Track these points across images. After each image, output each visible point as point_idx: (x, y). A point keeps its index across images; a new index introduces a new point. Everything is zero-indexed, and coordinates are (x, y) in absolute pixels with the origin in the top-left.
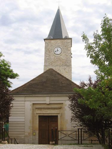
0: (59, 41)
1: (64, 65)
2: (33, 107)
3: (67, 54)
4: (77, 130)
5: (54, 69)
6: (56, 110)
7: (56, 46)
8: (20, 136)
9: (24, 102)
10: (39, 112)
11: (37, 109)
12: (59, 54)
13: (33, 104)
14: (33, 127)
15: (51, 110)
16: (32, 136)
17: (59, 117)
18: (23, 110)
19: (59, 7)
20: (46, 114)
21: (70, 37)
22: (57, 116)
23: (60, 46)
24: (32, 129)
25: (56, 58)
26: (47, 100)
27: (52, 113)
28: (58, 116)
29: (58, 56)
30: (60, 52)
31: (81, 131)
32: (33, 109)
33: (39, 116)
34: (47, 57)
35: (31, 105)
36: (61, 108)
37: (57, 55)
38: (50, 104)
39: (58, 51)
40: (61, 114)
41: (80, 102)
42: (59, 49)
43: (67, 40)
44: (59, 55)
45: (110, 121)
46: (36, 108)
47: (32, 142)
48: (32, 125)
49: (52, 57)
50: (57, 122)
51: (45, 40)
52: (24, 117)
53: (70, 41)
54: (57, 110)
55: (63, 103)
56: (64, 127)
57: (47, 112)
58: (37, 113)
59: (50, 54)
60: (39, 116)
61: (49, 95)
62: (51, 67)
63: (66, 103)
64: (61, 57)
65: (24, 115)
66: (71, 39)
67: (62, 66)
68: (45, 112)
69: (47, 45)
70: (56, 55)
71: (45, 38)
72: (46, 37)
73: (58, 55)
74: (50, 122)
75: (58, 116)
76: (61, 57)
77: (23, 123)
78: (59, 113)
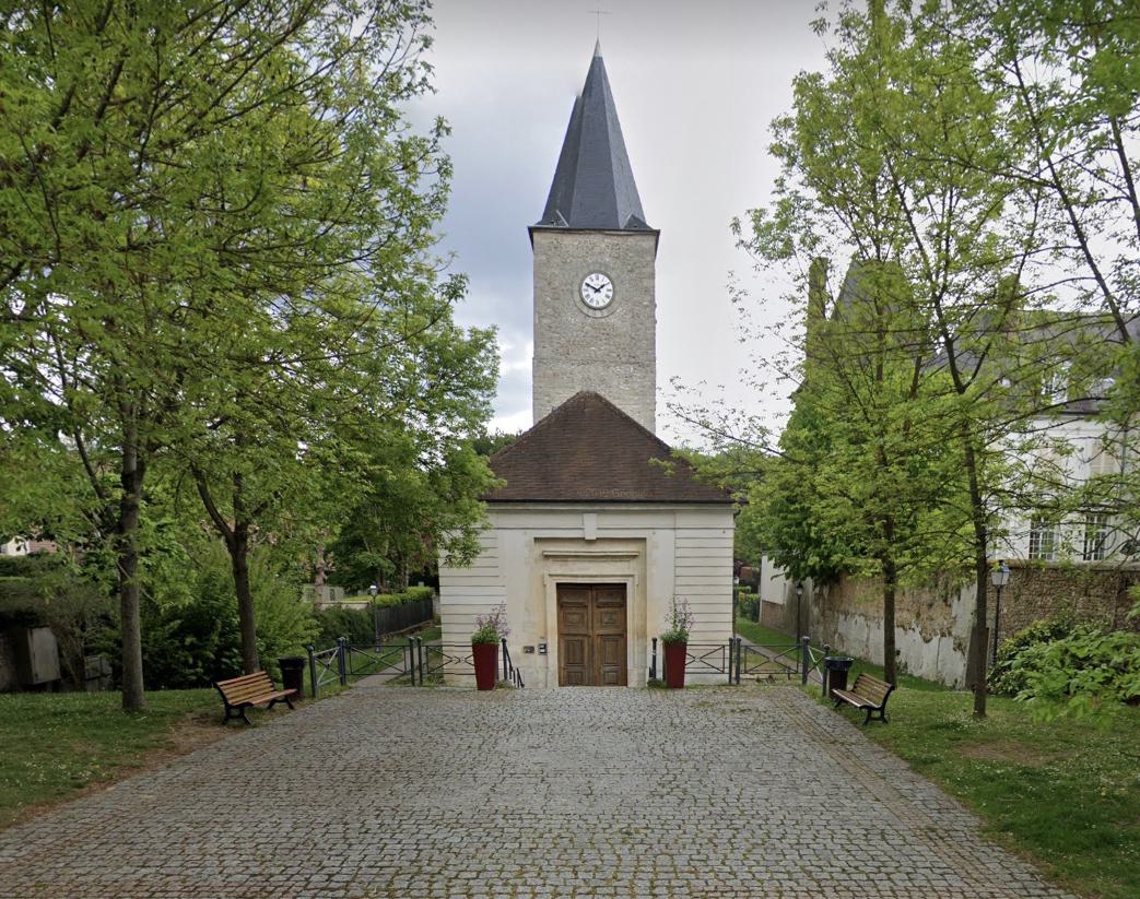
0: (601, 242)
1: (624, 359)
5: (602, 393)
6: (619, 564)
10: (559, 572)
12: (601, 304)
13: (536, 540)
19: (598, 42)
20: (583, 576)
21: (652, 223)
22: (623, 586)
23: (606, 266)
25: (590, 325)
26: (591, 525)
28: (625, 584)
29: (598, 314)
30: (607, 296)
34: (545, 321)
36: (635, 556)
37: (595, 309)
39: (597, 291)
41: (39, 606)
42: (607, 291)
44: (605, 312)
46: (546, 556)
49: (573, 319)
51: (531, 230)
53: (647, 242)
55: (644, 539)
60: (558, 585)
61: (597, 508)
64: (612, 320)
66: (657, 233)
67: (616, 364)
69: (544, 258)
70: (591, 313)
71: (532, 225)
72: (536, 217)
73: (600, 309)
75: (625, 584)
76: (612, 320)
78: (632, 576)
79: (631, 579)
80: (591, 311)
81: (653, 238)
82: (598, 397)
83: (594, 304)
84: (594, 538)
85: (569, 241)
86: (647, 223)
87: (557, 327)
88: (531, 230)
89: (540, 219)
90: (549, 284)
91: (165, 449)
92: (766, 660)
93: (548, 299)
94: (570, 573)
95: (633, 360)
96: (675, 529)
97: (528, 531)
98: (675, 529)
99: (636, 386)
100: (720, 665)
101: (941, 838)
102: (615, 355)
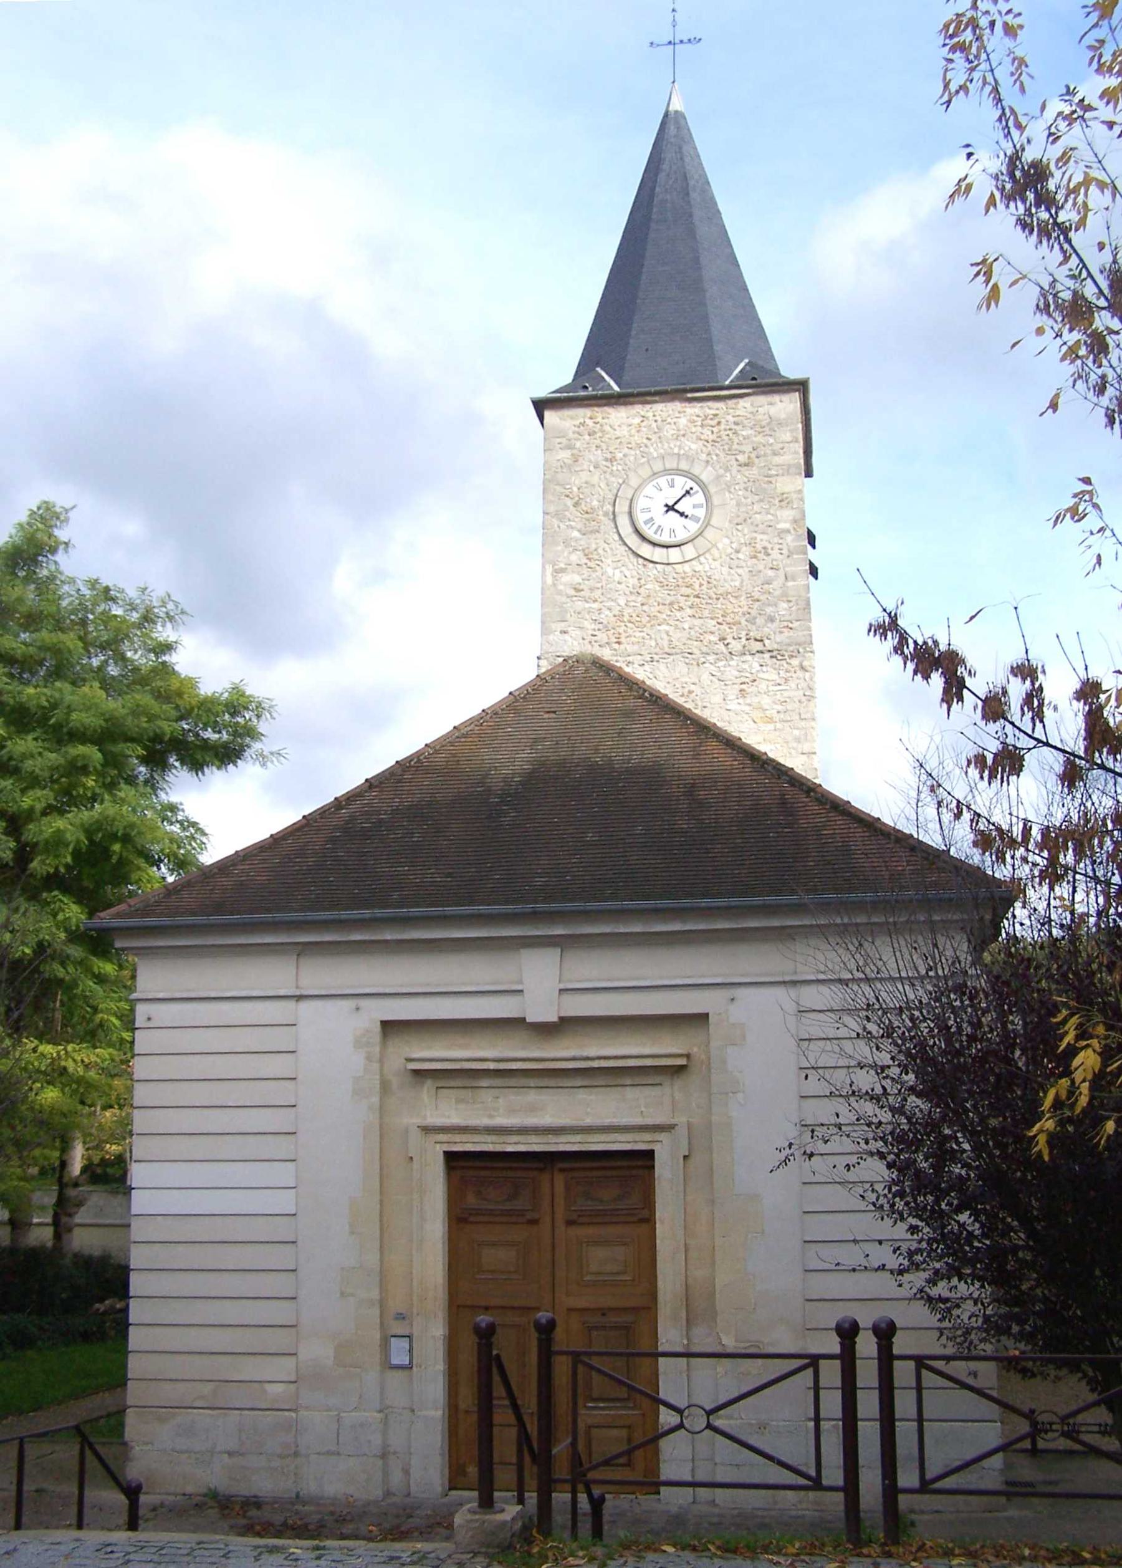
2: (381, 1061)
3: (762, 540)
4: (833, 1345)
6: (630, 1093)
7: (658, 466)
8: (250, 1369)
9: (291, 1004)
10: (455, 1120)
11: (429, 1083)
13: (388, 1026)
14: (383, 1277)
15: (582, 1095)
16: (372, 1376)
17: (665, 1169)
18: (281, 1093)
21: (789, 370)
23: (691, 459)
24: (375, 1294)
27: (588, 1121)
28: (649, 1155)
29: (674, 555)
31: (886, 1358)
32: (385, 1087)
33: (452, 1158)
34: (566, 578)
35: (358, 1044)
36: (681, 1069)
38: (564, 1026)
40: (682, 1132)
43: (761, 399)
44: (689, 551)
45: (1104, 2)
46: (417, 1072)
47: (377, 1440)
48: (372, 1259)
50: (649, 1220)
51: (541, 406)
52: (284, 1174)
54: (614, 1094)
55: (706, 1016)
56: (721, 1280)
57: (532, 1109)
58: (427, 1130)
59: (1052, 949)
60: (452, 1158)
61: (559, 931)
62: (573, 645)
63: (736, 1013)
65: (282, 1147)
66: (801, 387)
68: (511, 1111)
69: (565, 455)
70: (658, 554)
71: (542, 393)
74: (570, 1223)
75: (649, 1155)
77: (282, 1230)
78: (667, 1128)
79: (662, 1136)
80: (658, 550)
81: (796, 396)
82: (605, 668)
83: (665, 538)
84: (553, 1018)
85: (619, 418)
86: (783, 373)
87: (592, 590)
88: (541, 406)
89: (567, 378)
90: (576, 505)
91: (1046, 1292)
92: (719, 1422)
93: (576, 534)
94: (485, 1121)
95: (758, 646)
96: (794, 983)
97: (365, 1003)
98: (794, 983)
99: (766, 701)
100: (800, 1453)
101: (1011, 814)
102: (714, 638)
